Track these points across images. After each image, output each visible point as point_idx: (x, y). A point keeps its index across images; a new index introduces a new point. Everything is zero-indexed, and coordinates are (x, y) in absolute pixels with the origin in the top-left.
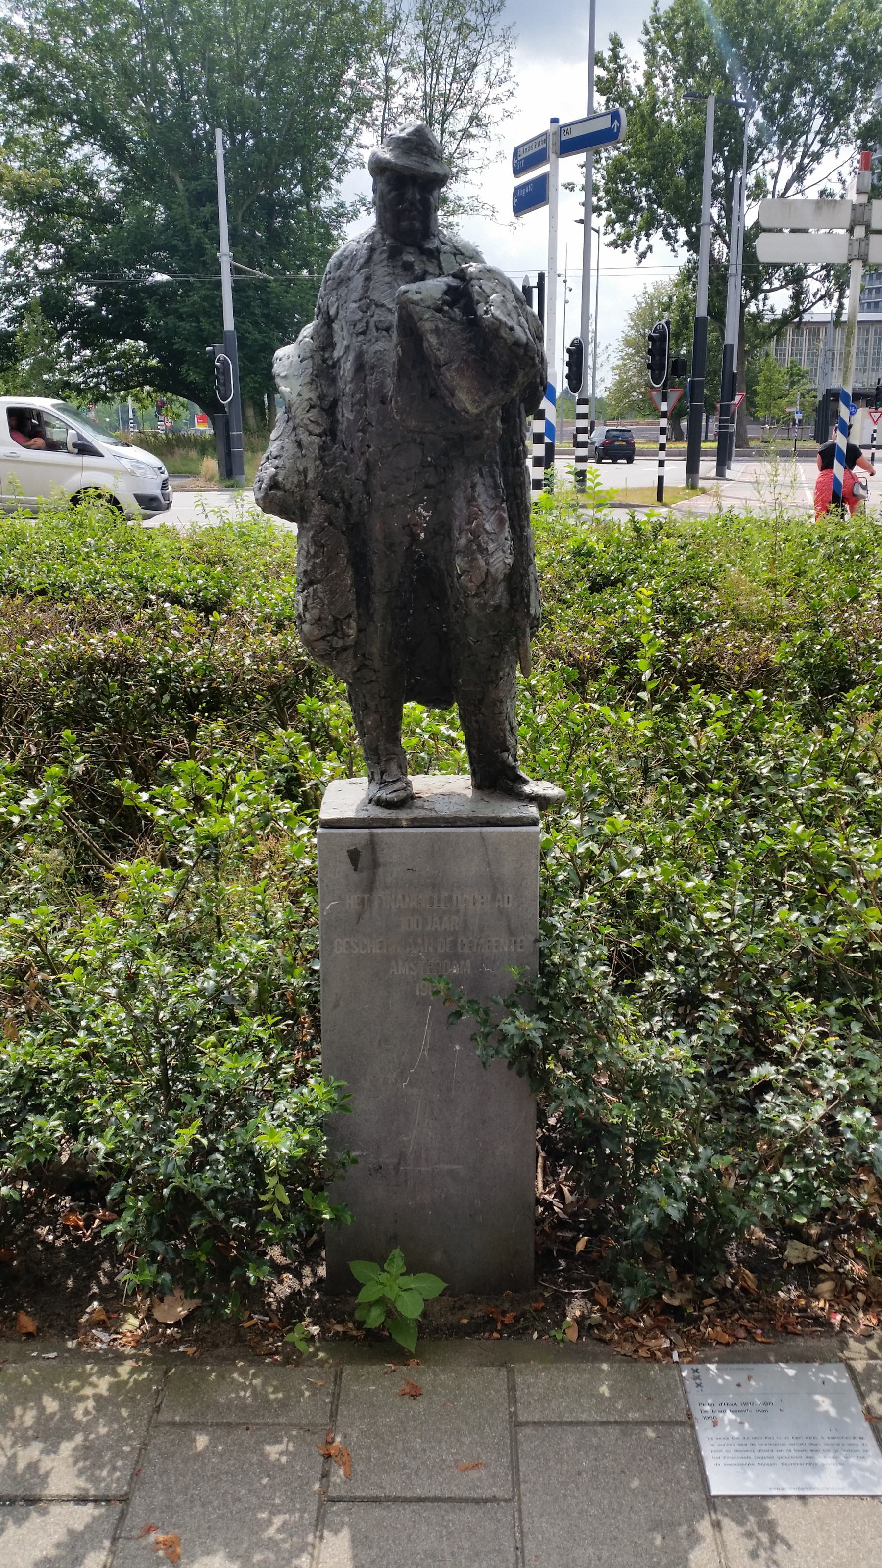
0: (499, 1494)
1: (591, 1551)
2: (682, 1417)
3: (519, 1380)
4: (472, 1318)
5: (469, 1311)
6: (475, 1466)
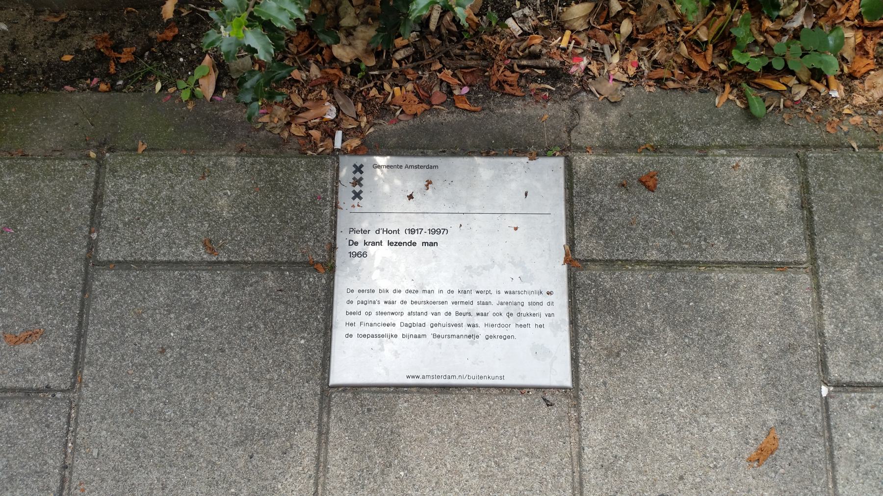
0: (54, 384)
1: (155, 474)
2: (319, 256)
3: (110, 185)
4: (78, 51)
5: (76, 41)
6: (29, 337)
